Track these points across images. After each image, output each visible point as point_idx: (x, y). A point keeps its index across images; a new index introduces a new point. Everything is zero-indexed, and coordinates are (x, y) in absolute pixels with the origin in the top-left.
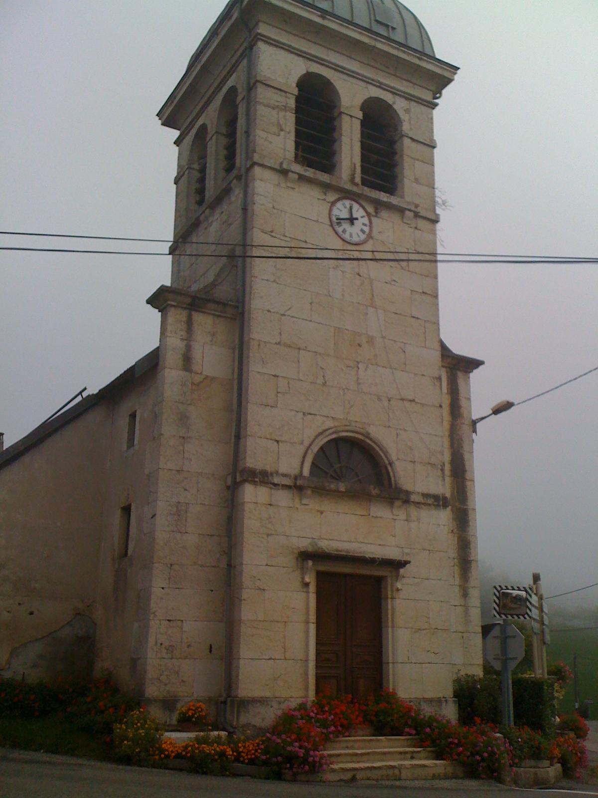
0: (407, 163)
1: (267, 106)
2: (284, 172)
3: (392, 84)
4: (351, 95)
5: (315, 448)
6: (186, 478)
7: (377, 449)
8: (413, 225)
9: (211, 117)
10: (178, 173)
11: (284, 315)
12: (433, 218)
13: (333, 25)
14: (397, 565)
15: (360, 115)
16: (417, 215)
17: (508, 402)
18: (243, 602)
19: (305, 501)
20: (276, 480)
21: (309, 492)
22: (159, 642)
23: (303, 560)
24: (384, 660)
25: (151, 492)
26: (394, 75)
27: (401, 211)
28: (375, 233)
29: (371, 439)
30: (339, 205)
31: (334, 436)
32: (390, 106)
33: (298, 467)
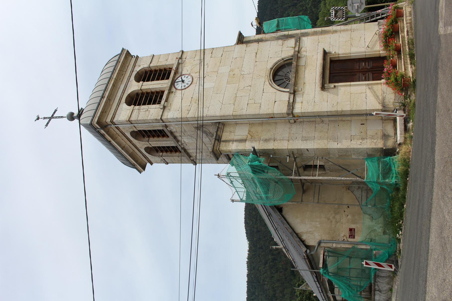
1: (138, 116)
2: (164, 107)
3: (129, 72)
4: (135, 86)
5: (278, 87)
8: (185, 59)
9: (142, 145)
12: (181, 53)
13: (107, 94)
14: (325, 53)
15: (141, 82)
16: (181, 58)
19: (300, 90)
20: (291, 101)
21: (296, 88)
22: (360, 144)
27: (179, 64)
28: (188, 73)
29: (273, 67)
30: (176, 87)
31: (272, 81)
32: (138, 72)
33: (286, 93)
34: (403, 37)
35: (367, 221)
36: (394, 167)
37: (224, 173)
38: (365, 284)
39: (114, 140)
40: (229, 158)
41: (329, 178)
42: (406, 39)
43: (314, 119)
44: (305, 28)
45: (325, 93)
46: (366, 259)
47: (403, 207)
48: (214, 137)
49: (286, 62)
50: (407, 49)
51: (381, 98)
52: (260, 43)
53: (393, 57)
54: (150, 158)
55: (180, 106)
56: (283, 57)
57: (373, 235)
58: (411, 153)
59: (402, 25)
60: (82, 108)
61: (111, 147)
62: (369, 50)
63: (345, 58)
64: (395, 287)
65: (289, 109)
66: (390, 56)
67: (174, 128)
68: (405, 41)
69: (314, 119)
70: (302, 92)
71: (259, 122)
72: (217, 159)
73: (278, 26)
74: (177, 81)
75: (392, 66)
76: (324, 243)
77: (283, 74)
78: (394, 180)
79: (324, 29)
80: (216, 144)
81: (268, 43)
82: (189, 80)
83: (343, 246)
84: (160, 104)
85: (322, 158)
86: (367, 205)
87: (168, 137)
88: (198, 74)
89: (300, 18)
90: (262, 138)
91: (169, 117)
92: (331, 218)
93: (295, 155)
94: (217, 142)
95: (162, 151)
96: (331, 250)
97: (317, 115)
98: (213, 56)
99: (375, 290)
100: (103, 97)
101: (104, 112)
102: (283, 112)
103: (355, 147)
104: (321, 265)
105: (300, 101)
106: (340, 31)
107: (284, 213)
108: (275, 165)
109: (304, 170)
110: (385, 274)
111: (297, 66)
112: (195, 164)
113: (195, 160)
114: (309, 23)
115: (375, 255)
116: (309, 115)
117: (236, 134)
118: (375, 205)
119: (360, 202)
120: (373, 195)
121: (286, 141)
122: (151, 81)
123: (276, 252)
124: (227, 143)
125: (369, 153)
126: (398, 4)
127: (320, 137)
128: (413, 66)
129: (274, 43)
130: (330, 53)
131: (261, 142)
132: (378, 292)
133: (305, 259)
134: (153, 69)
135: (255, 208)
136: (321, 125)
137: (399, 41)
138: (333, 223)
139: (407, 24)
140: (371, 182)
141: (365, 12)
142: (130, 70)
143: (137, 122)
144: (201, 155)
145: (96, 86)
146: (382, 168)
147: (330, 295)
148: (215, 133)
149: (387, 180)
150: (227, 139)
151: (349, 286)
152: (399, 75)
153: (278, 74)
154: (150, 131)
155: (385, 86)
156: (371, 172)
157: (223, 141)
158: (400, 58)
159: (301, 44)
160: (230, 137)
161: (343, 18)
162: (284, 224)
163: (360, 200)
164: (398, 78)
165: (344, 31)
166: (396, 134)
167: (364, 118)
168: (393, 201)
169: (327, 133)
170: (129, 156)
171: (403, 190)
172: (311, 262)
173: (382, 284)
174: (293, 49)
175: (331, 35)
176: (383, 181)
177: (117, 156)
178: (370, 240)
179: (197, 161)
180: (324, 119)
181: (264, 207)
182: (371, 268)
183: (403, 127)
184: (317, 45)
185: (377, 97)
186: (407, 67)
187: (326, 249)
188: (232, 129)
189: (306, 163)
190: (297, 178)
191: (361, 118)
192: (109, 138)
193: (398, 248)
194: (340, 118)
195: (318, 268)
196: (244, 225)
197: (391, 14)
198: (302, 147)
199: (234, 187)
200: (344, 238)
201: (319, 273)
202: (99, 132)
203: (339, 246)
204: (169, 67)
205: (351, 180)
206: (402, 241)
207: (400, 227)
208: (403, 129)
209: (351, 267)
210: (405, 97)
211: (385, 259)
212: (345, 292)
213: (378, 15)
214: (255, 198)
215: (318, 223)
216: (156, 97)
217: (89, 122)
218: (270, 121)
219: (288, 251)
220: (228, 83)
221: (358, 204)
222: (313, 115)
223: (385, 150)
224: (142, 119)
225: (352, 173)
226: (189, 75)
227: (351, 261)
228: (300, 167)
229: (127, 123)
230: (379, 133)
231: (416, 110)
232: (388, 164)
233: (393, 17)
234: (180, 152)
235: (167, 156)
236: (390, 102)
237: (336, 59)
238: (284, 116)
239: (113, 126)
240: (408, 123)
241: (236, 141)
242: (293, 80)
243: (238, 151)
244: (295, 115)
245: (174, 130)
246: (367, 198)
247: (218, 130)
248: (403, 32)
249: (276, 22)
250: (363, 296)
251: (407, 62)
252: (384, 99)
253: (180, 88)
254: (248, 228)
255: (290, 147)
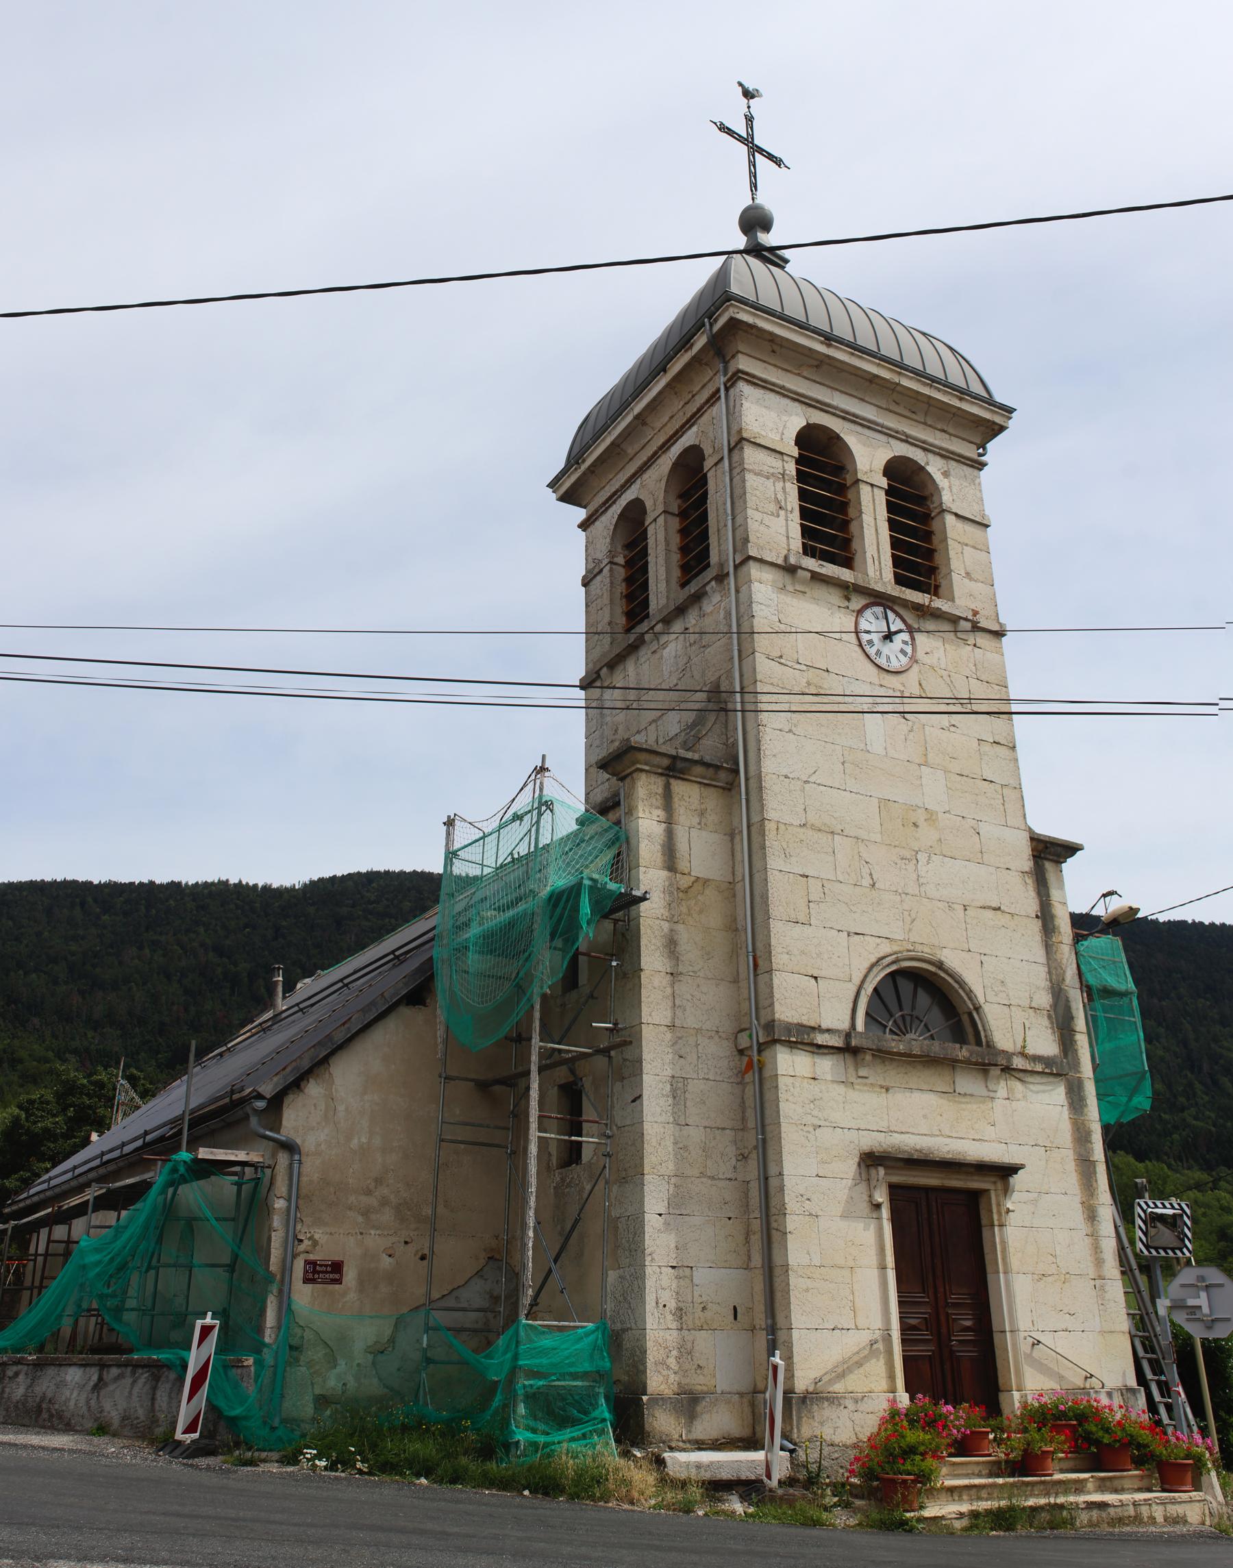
0: (953, 549)
2: (790, 569)
4: (869, 457)
5: (869, 988)
6: (680, 1038)
7: (956, 986)
8: (971, 641)
9: (653, 488)
10: (588, 571)
11: (806, 782)
12: (996, 628)
13: (841, 355)
14: (1005, 1172)
15: (884, 482)
16: (976, 628)
17: (1131, 908)
18: (789, 1236)
19: (862, 1072)
20: (820, 1039)
21: (868, 1057)
23: (868, 1166)
24: (995, 1327)
25: (625, 1060)
26: (925, 424)
27: (954, 620)
28: (920, 655)
30: (868, 613)
31: (894, 968)
32: (922, 469)
34: (1079, 1487)
35: (366, 1333)
36: (573, 1439)
37: (551, 790)
38: (130, 1324)
39: (668, 385)
40: (608, 808)
41: (533, 1180)
42: (1072, 1499)
43: (751, 1124)
44: (1100, 1097)
45: (850, 1167)
46: (224, 1328)
47: (418, 1475)
48: (682, 753)
49: (965, 1018)
50: (1031, 1502)
51: (838, 1387)
52: (1039, 923)
53: (998, 1442)
54: (603, 518)
55: (796, 630)
56: (987, 1009)
57: (315, 1354)
58: (626, 1506)
59: (1127, 1484)
60: (787, 261)
61: (644, 374)
62: (1025, 1347)
63: (987, 1250)
64: (110, 1447)
65: (788, 1028)
66: (1003, 1431)
67: (716, 605)
68: (1066, 1492)
69: (751, 1124)
70: (853, 1079)
71: (740, 918)
72: (604, 765)
73: (1107, 992)
74: (891, 615)
75: (965, 1437)
76: (291, 1165)
77: (921, 1013)
78: (521, 1436)
79: (1101, 1170)
80: (657, 760)
81: (1040, 954)
82: (893, 659)
83: (276, 1240)
84: (805, 553)
85: (608, 1155)
86: (428, 1329)
87: (683, 585)
88: (917, 692)
89: (1143, 1077)
90: (680, 927)
91: (756, 586)
92: (385, 1191)
93: (621, 1050)
94: (666, 762)
95: (629, 564)
96: (263, 1190)
97: (769, 1135)
98: (986, 748)
99: (103, 1366)
100: (829, 339)
101: (774, 347)
102: (777, 1007)
103: (650, 1284)
104: (204, 1153)
105: (819, 1074)
106: (1094, 1236)
107: (406, 1011)
108: (583, 978)
109: (561, 1087)
110: (164, 1405)
111: (952, 1064)
112: (585, 685)
113: (598, 684)
114: (1123, 1113)
115: (238, 1364)
116: (767, 1105)
117: (694, 833)
118: (429, 1361)
119: (442, 1304)
120: (468, 1355)
121: (670, 1016)
122: (890, 520)
123: (263, 990)
124: (659, 801)
125: (626, 1336)
126: (1213, 1473)
127: (685, 1148)
128: (965, 1522)
129: (1039, 976)
130: (1007, 1190)
131: (666, 926)
132: (95, 1378)
133: (232, 1092)
134: (935, 525)
135: (424, 909)
136: (731, 1151)
137: (1062, 1471)
138: (364, 1199)
139: (1135, 1504)
140: (518, 1342)
141: (1175, 1336)
142: (931, 440)
143: (737, 471)
144: (619, 704)
145: (872, 315)
146: (570, 1390)
147: (89, 1195)
148: (696, 757)
149: (522, 1409)
150: (676, 800)
151: (122, 1267)
152: (930, 1462)
153: (920, 991)
154: (704, 517)
155: (885, 1405)
156: (554, 1346)
157: (667, 787)
158: (997, 1469)
159: (1038, 1079)
160: (682, 810)
161: (1147, 1247)
162: (363, 1011)
163: (451, 1303)
164: (918, 1458)
165: (1097, 1249)
166: (700, 1445)
167: (760, 1320)
168: (443, 1435)
169: (702, 1174)
170: (612, 443)
171: (485, 1474)
172: (221, 1118)
173: (124, 1396)
174: (1019, 1049)
175: (1078, 1199)
176: (521, 1392)
177: (611, 395)
178: (294, 1342)
179: (596, 693)
180: (753, 1164)
181: (429, 939)
182: (189, 1348)
183: (725, 1475)
184: (1037, 1142)
185: (842, 1372)
186: (960, 1499)
187: (268, 1171)
188: (712, 818)
189: (592, 1082)
190: (534, 1058)
191: (760, 1308)
192: (676, 367)
193: (264, 1455)
194: (756, 1225)
195: (193, 1145)
196: (364, 870)
197: (1173, 1439)
198: (647, 1079)
199: (500, 827)
200: (306, 1242)
201: (177, 1149)
202: (699, 326)
203: (277, 1222)
204: (944, 583)
205: (524, 1266)
206: (290, 1469)
207: (344, 1464)
208: (718, 1477)
209: (195, 1270)
210: (843, 1485)
211: (221, 1403)
212: (97, 1250)
213: (1165, 1389)
214: (459, 907)
215: (364, 1140)
216: (830, 540)
217: (735, 289)
218: (742, 959)
219: (264, 1029)
220: (884, 802)
221: (436, 1295)
222: (767, 1121)
223: (638, 1404)
224: (748, 489)
225: (550, 1271)
226: (914, 660)
227: (220, 1270)
228: (572, 1072)
229: (734, 432)
230: (701, 1380)
231: (793, 1530)
232: (586, 1413)
233: (1161, 1451)
234: (628, 630)
235: (611, 583)
236: (822, 1423)
237: (983, 1213)
238: (762, 1012)
239: (723, 379)
240: (743, 1499)
241: (670, 835)
242: (897, 1044)
243: (633, 841)
244: (767, 1054)
245: (707, 606)
246: (457, 1331)
247: (708, 765)
248: (1102, 1486)
249: (1122, 988)
250: (82, 1321)
251: (979, 1499)
252: (834, 1400)
253: (864, 625)
254: (350, 883)
255: (647, 1033)
